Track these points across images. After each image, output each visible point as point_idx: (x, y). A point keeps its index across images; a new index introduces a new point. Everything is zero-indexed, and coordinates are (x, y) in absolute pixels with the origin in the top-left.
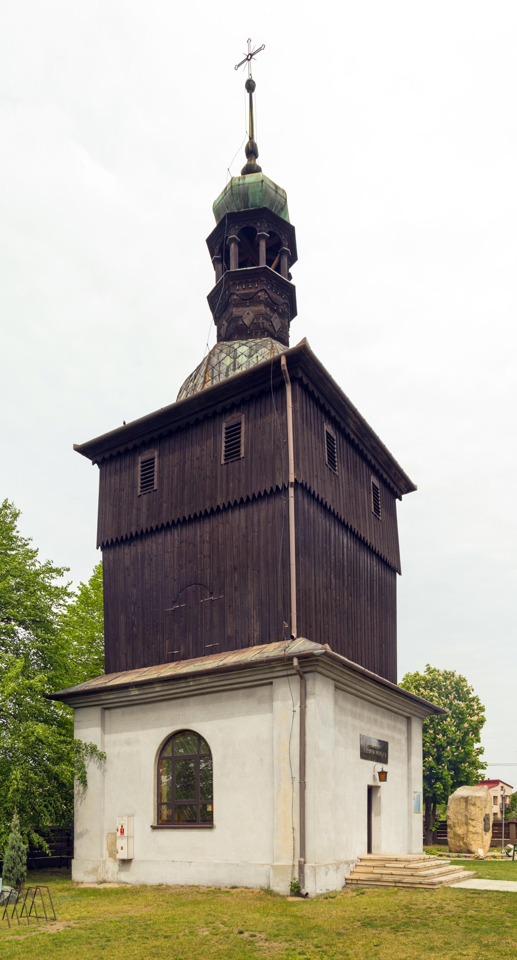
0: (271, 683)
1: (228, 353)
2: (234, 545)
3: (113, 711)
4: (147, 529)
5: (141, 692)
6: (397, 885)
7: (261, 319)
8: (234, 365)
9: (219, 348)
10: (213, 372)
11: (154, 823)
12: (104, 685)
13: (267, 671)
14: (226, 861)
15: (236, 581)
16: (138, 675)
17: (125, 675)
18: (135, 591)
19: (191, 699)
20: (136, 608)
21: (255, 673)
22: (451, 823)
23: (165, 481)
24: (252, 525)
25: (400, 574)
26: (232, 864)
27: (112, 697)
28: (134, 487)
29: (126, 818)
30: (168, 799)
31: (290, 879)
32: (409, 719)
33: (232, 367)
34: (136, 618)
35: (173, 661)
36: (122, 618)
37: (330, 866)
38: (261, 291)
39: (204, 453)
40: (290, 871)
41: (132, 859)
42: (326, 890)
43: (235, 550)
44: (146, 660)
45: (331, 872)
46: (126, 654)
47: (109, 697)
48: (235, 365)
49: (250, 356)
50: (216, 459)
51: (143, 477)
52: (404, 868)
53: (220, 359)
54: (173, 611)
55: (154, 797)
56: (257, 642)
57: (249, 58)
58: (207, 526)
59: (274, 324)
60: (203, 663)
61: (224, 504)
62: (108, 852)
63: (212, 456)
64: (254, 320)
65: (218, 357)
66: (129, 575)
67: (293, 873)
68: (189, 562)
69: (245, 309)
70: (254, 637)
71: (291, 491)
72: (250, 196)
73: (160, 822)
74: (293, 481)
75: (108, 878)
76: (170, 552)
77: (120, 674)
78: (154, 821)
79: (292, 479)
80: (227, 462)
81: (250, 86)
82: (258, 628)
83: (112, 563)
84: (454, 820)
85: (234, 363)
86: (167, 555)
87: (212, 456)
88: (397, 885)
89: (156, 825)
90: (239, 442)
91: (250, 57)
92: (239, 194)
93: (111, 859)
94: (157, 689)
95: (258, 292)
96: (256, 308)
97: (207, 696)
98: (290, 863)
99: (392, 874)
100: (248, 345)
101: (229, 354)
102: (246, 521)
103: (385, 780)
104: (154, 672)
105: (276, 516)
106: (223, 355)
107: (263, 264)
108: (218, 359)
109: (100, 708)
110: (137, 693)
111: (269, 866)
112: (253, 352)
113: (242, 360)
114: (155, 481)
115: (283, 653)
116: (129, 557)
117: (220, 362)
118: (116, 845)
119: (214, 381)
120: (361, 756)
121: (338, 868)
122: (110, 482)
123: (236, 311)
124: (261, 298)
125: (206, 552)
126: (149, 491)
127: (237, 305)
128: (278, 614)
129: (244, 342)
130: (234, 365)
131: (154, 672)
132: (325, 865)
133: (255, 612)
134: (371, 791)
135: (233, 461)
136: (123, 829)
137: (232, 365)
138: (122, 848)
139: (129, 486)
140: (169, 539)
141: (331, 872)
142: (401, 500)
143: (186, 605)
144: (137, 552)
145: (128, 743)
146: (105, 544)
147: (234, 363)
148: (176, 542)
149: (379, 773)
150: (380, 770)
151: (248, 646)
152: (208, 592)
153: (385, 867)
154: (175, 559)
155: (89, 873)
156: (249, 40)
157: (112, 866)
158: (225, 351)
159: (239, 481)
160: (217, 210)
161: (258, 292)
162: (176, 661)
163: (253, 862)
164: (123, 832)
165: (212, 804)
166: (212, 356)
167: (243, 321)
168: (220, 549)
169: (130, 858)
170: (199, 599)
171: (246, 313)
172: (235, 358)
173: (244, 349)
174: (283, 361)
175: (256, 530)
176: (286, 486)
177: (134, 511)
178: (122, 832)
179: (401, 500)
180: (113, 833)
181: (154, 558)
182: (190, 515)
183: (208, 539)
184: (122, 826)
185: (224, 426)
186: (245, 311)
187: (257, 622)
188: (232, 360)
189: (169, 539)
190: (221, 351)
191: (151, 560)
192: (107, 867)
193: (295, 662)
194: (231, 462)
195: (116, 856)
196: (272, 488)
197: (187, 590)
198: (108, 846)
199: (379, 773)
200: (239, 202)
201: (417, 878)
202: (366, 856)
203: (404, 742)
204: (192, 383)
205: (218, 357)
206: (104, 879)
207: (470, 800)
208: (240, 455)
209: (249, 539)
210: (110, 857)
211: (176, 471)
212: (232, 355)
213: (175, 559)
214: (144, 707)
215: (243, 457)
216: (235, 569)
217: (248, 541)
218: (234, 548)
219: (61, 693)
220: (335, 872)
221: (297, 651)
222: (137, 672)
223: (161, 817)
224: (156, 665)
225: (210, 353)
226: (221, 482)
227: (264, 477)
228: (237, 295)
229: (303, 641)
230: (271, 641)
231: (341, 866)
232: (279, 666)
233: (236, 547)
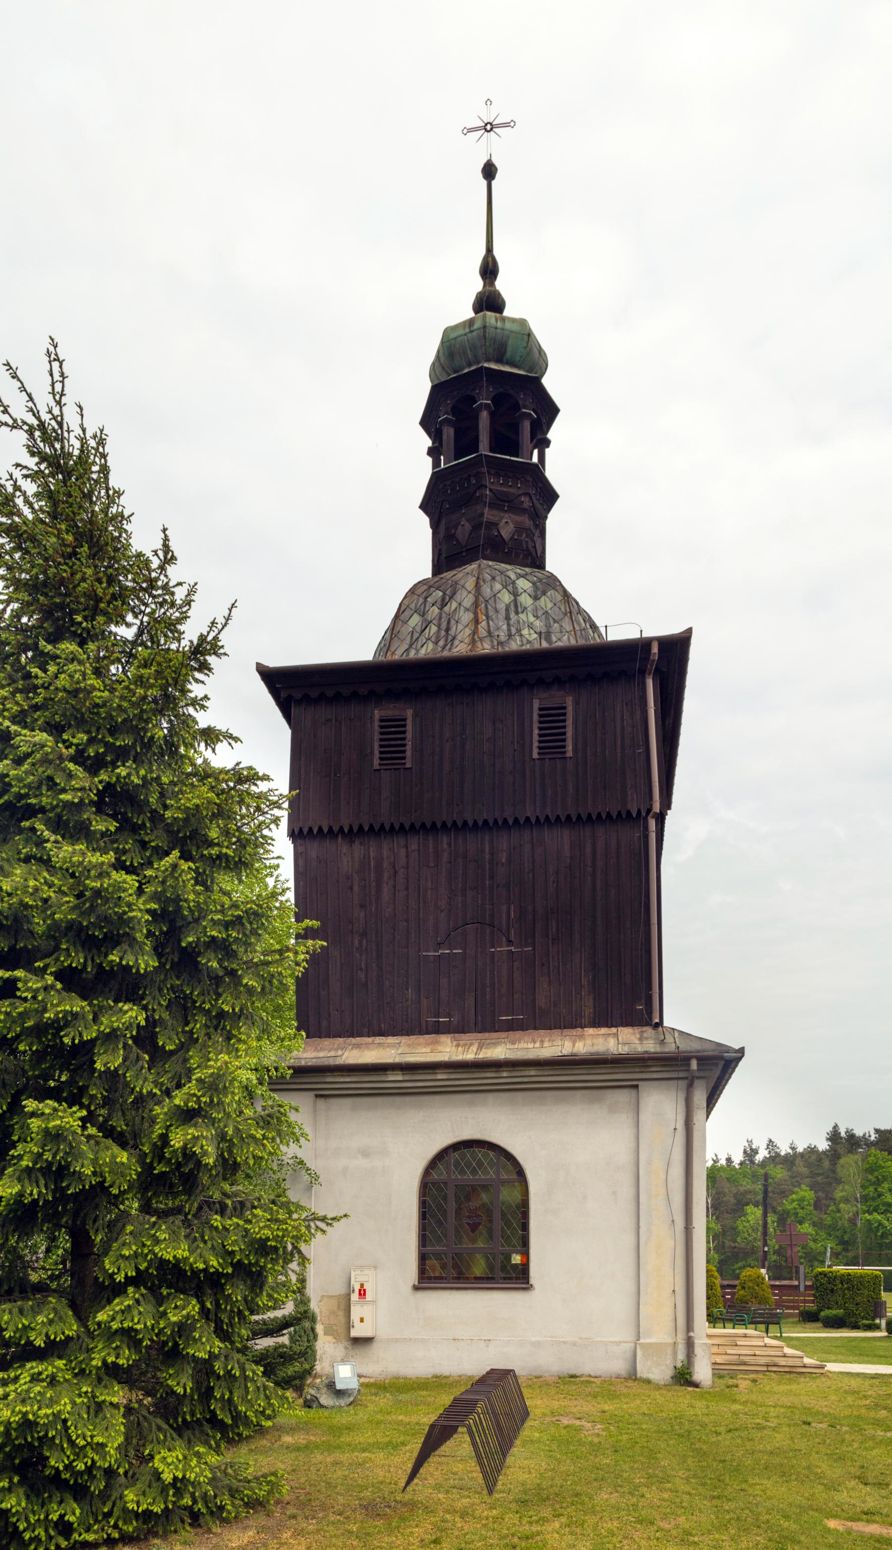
5: (407, 1078)
6: (770, 1369)
7: (524, 535)
8: (516, 607)
13: (637, 1070)
19: (490, 1096)
21: (617, 1071)
26: (564, 1343)
31: (669, 1362)
33: (512, 607)
34: (364, 957)
38: (524, 494)
40: (669, 1351)
52: (765, 1346)
64: (514, 535)
67: (675, 1354)
72: (509, 349)
74: (658, 811)
85: (515, 601)
88: (770, 1369)
92: (494, 340)
95: (520, 495)
96: (518, 518)
97: (520, 1095)
98: (670, 1340)
99: (755, 1355)
108: (492, 590)
109: (312, 1093)
110: (400, 1078)
117: (495, 595)
130: (516, 607)
136: (365, 1290)
137: (512, 604)
138: (362, 1320)
143: (464, 953)
145: (365, 1153)
152: (504, 939)
153: (736, 1345)
156: (489, 103)
160: (450, 347)
161: (520, 495)
163: (600, 1339)
164: (365, 1294)
167: (498, 531)
170: (488, 946)
174: (655, 649)
176: (644, 814)
178: (362, 1293)
183: (504, 860)
184: (362, 1285)
185: (536, 704)
186: (502, 518)
188: (513, 598)
193: (694, 1064)
200: (491, 350)
201: (790, 1359)
208: (565, 752)
214: (398, 1099)
232: (657, 1066)
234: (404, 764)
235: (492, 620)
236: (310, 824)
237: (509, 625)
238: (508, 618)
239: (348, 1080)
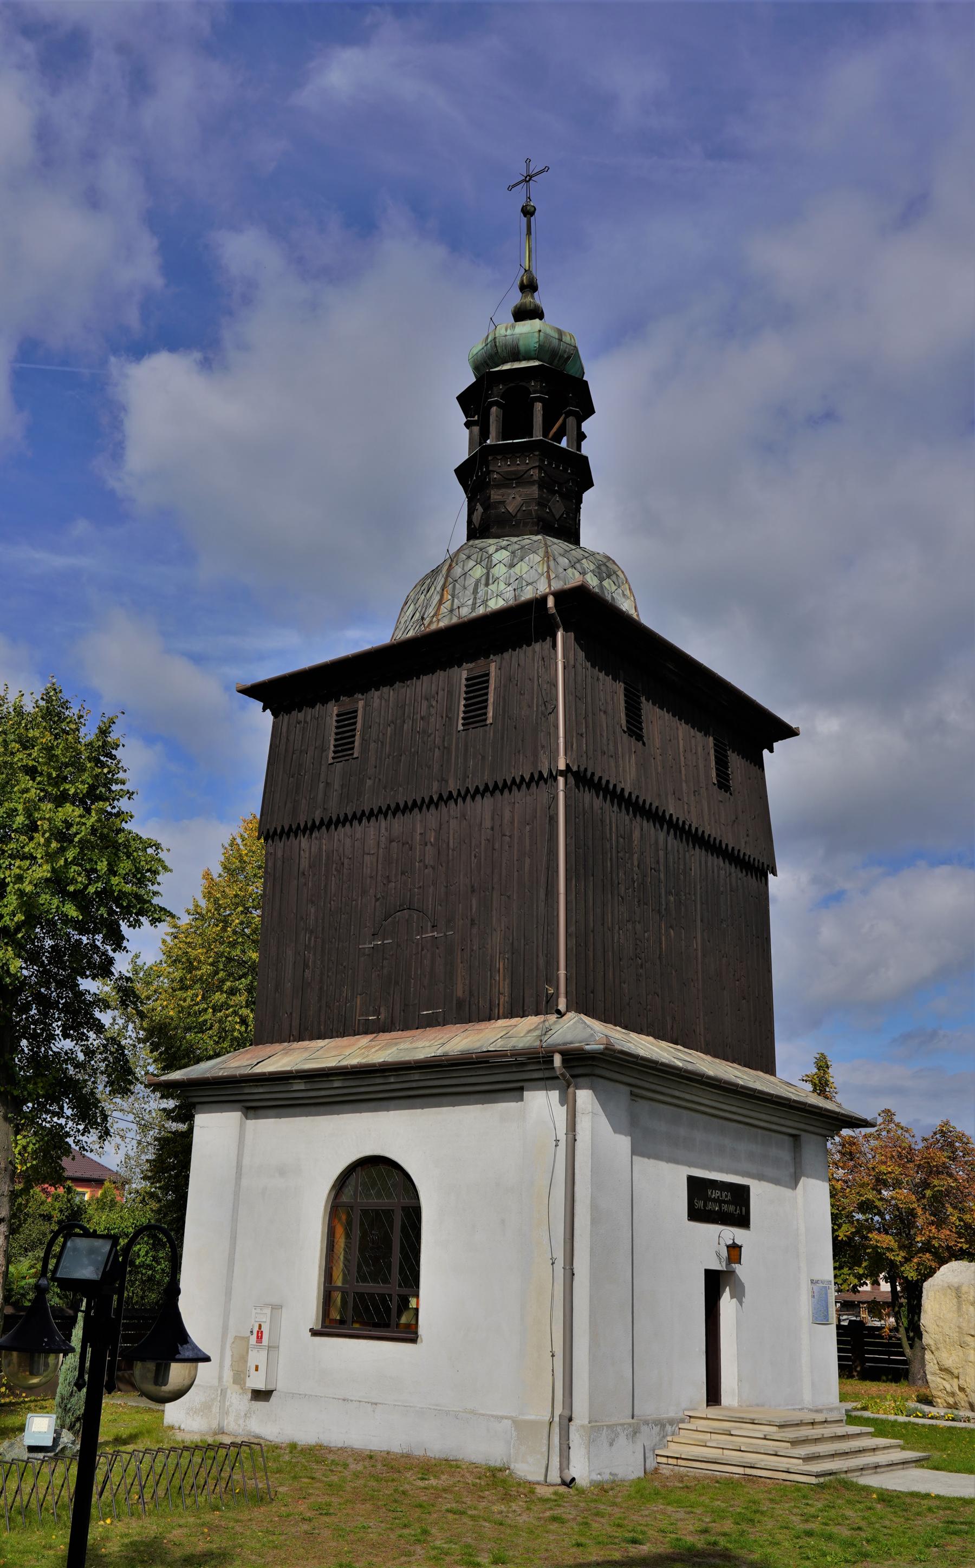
1: (479, 560)
2: (473, 854)
4: (338, 815)
5: (309, 1087)
9: (467, 552)
11: (317, 1323)
12: (247, 1071)
14: (437, 1405)
15: (474, 910)
16: (306, 1055)
17: (287, 1052)
18: (313, 910)
20: (313, 938)
22: (931, 1342)
23: (373, 745)
24: (501, 825)
25: (775, 874)
27: (261, 1090)
28: (323, 749)
29: (268, 1311)
30: (345, 1281)
33: (483, 581)
35: (366, 1032)
36: (290, 953)
37: (619, 1429)
38: (533, 468)
39: (433, 711)
41: (272, 1391)
42: (611, 1474)
43: (474, 861)
44: (322, 1027)
45: (622, 1440)
46: (291, 1013)
49: (512, 566)
50: (449, 719)
51: (339, 737)
53: (466, 569)
54: (371, 950)
55: (320, 1274)
56: (504, 1012)
57: (527, 179)
58: (432, 817)
59: (553, 510)
60: (414, 1045)
61: (459, 790)
62: (232, 1373)
63: (444, 716)
65: (463, 566)
66: (305, 884)
68: (402, 874)
69: (509, 491)
70: (499, 1004)
71: (561, 780)
73: (327, 1323)
75: (228, 1425)
76: (373, 854)
77: (277, 1047)
78: (317, 1319)
79: (562, 766)
80: (466, 727)
81: (528, 212)
82: (506, 990)
83: (279, 863)
84: (936, 1336)
85: (488, 574)
86: (367, 858)
87: (444, 716)
89: (318, 1327)
90: (486, 700)
91: (528, 178)
93: (237, 1387)
94: (336, 1084)
100: (510, 548)
101: (481, 561)
102: (493, 819)
104: (333, 1053)
105: (538, 814)
107: (538, 436)
110: (302, 1087)
111: (509, 1422)
112: (515, 561)
114: (357, 744)
115: (537, 1043)
116: (307, 855)
118: (246, 1362)
119: (456, 600)
120: (689, 1216)
121: (635, 1433)
122: (287, 739)
123: (495, 495)
124: (534, 477)
125: (429, 860)
126: (347, 758)
127: (499, 486)
128: (537, 969)
129: (505, 543)
131: (333, 1053)
132: (608, 1426)
133: (501, 964)
135: (477, 727)
136: (262, 1332)
137: (484, 578)
138: (257, 1369)
139: (315, 748)
140: (372, 833)
141: (622, 1440)
142: (771, 751)
144: (320, 849)
147: (488, 574)
148: (383, 839)
149: (728, 1247)
150: (730, 1242)
151: (490, 1020)
152: (429, 923)
154: (380, 866)
155: (195, 1412)
157: (239, 1401)
158: (474, 557)
159: (483, 757)
162: (372, 1033)
165: (417, 1296)
166: (454, 564)
168: (451, 857)
169: (270, 1388)
171: (511, 498)
172: (489, 567)
173: (504, 555)
174: (551, 602)
175: (507, 834)
176: (554, 773)
177: (322, 786)
178: (260, 1338)
179: (771, 751)
180: (243, 1338)
181: (346, 861)
182: (406, 802)
183: (432, 840)
184: (260, 1326)
187: (504, 980)
189: (372, 833)
190: (469, 557)
191: (343, 864)
192: (227, 1404)
194: (473, 728)
195: (245, 1383)
196: (532, 774)
197: (395, 918)
198: (232, 1360)
199: (728, 1247)
202: (703, 1409)
204: (423, 596)
205: (463, 566)
206: (221, 1426)
207: (966, 1293)
208: (485, 720)
209: (497, 846)
210: (234, 1382)
211: (389, 733)
212: (484, 563)
213: (380, 866)
215: (491, 724)
216: (473, 891)
217: (494, 849)
218: (473, 857)
219: (178, 1077)
220: (630, 1440)
221: (560, 1041)
222: (306, 1049)
223: (328, 1317)
224: (338, 1037)
226: (457, 757)
227: (521, 757)
229: (576, 1018)
230: (527, 1013)
231: (644, 1429)
233: (475, 857)
234: (352, 754)
235: (458, 598)
236: (622, 785)
237: (475, 599)
238: (475, 592)
239: (261, 1090)
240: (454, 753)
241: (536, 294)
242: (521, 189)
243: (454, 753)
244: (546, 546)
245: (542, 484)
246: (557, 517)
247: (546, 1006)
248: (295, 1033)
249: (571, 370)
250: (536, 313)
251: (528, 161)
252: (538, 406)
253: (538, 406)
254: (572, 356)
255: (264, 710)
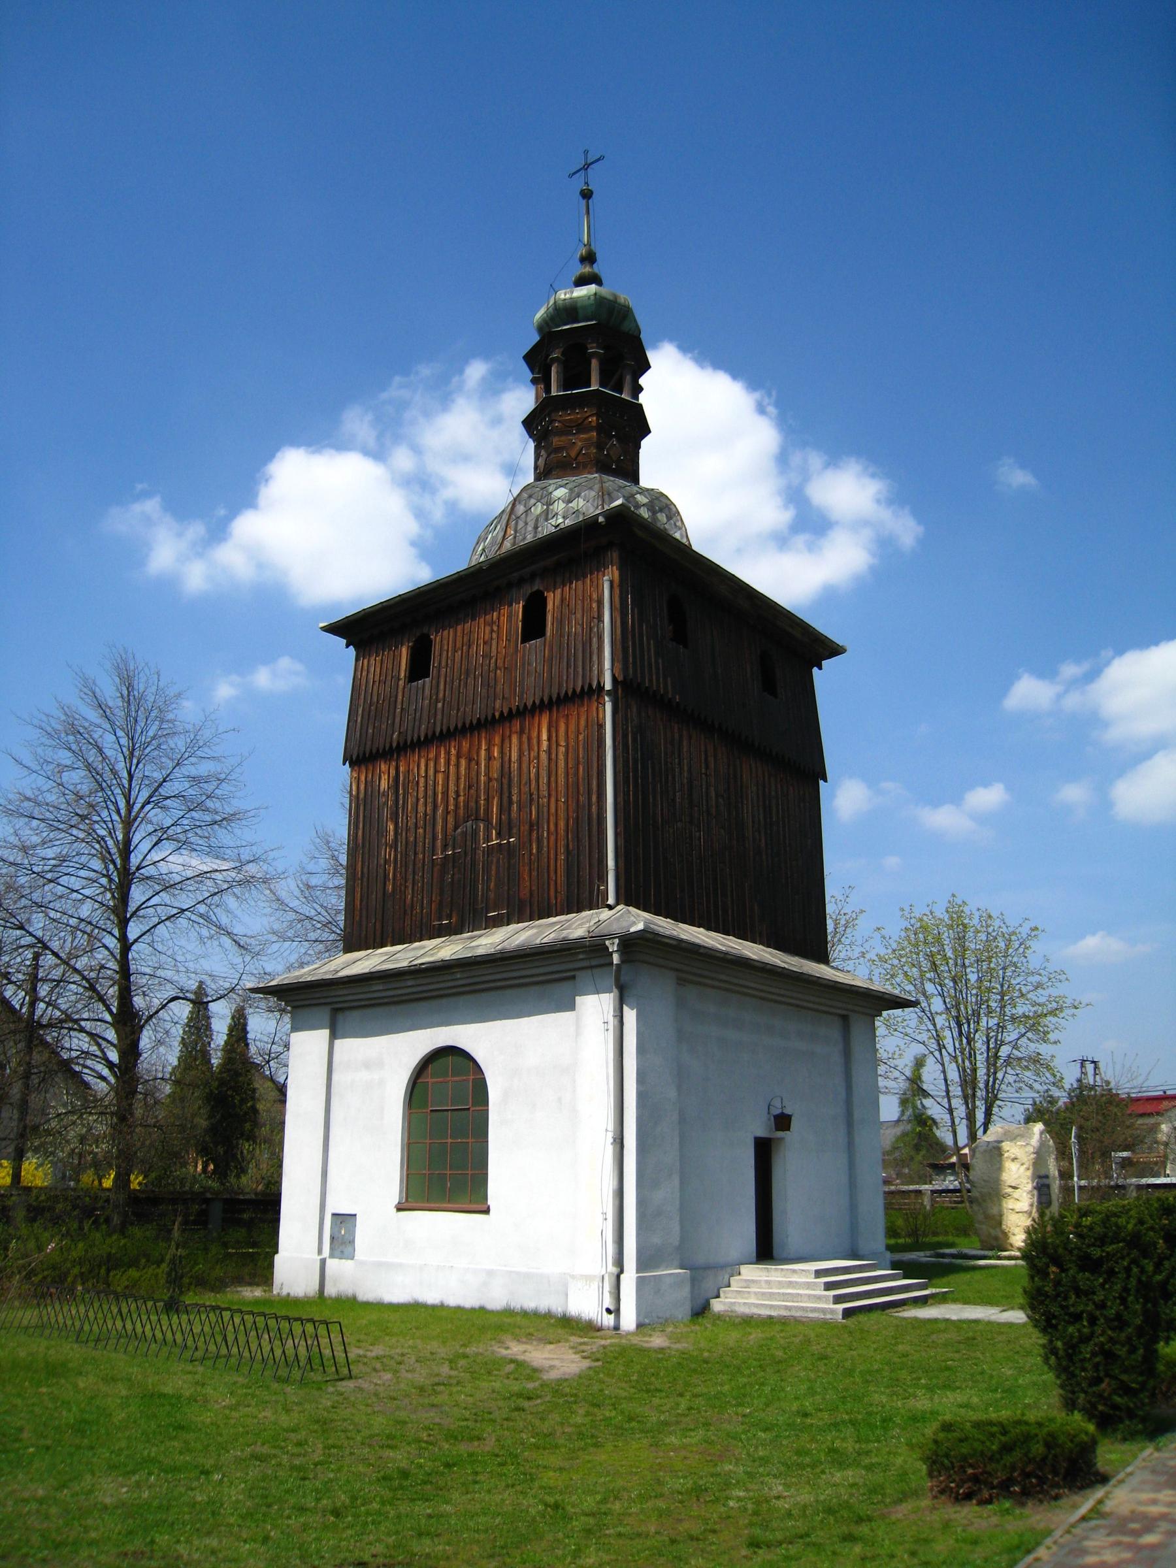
0: (574, 977)
3: (348, 1013)
10: (517, 524)
19: (462, 998)
25: (826, 781)
32: (845, 1018)
47: (341, 993)
48: (546, 515)
49: (570, 501)
91: (586, 167)
94: (410, 983)
103: (788, 1128)
106: (533, 501)
110: (381, 987)
113: (560, 507)
134: (764, 1151)
142: (820, 668)
145: (367, 1065)
146: (354, 758)
161: (588, 417)
172: (549, 504)
173: (561, 492)
179: (820, 668)
190: (530, 497)
203: (837, 1058)
212: (544, 500)
214: (393, 1008)
225: (515, 500)
228: (559, 422)
240: (581, 747)
241: (595, 266)
242: (581, 176)
243: (581, 747)
244: (602, 482)
245: (599, 429)
246: (614, 458)
247: (595, 901)
248: (378, 940)
249: (626, 326)
250: (595, 279)
251: (586, 152)
252: (595, 364)
253: (595, 364)
254: (625, 313)
255: (347, 646)
